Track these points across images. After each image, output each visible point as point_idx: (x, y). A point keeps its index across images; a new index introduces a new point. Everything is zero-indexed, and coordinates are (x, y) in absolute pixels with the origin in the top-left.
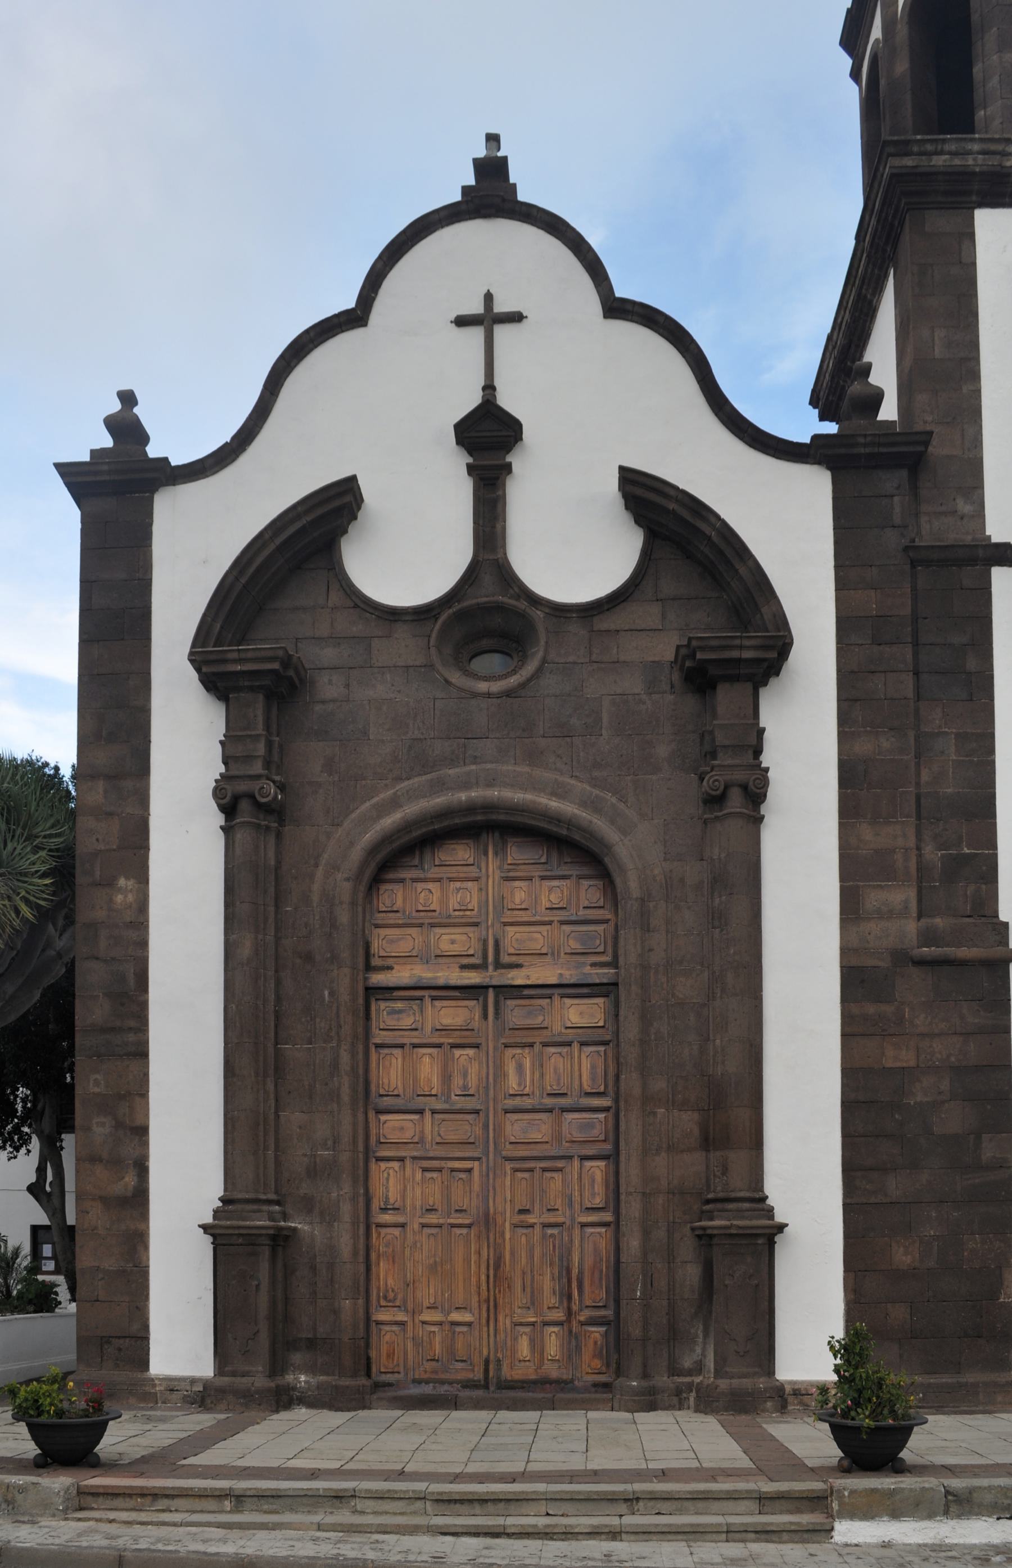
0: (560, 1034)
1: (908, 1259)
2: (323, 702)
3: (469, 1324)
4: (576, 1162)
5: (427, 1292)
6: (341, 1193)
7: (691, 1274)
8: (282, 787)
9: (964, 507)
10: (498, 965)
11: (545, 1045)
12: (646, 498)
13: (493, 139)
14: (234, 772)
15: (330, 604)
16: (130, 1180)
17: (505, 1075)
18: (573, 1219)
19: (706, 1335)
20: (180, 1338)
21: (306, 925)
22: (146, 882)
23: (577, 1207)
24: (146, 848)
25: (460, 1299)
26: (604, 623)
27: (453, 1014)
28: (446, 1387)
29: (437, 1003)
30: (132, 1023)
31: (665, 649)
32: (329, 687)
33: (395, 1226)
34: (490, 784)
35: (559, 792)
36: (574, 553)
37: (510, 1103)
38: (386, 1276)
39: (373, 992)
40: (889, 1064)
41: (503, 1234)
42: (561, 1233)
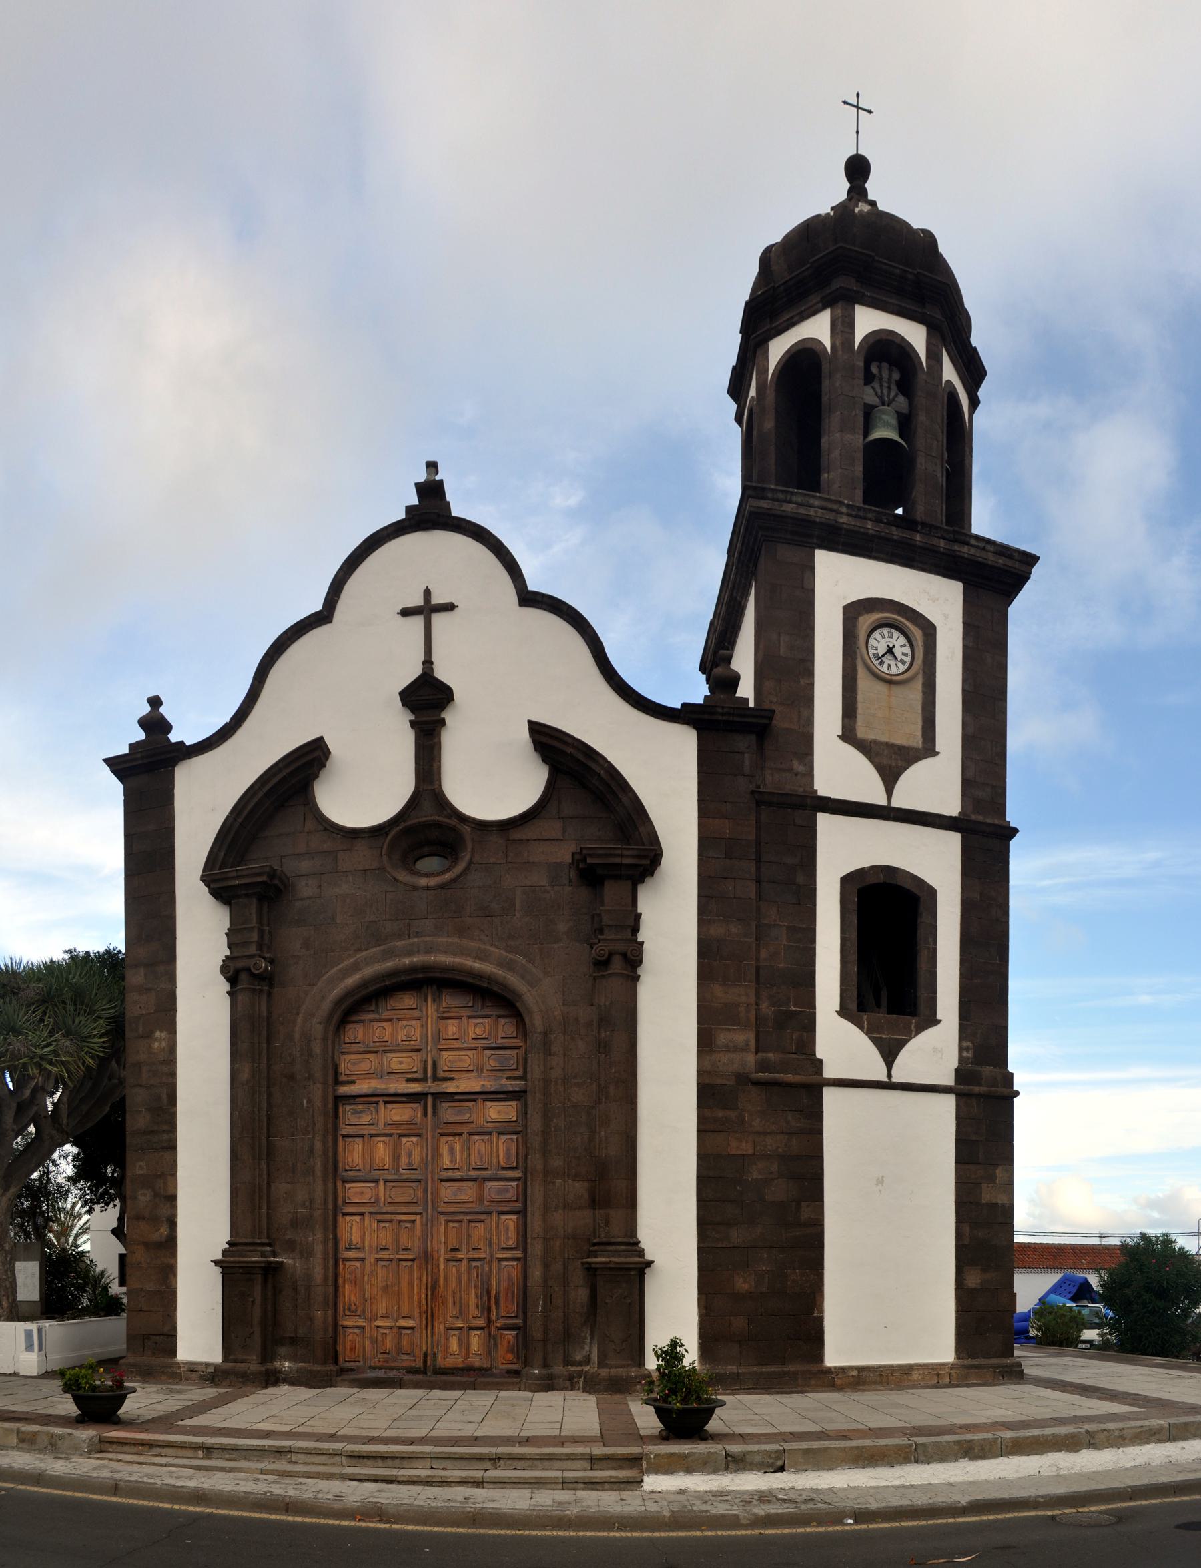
0: (483, 1126)
1: (746, 1286)
2: (302, 899)
3: (412, 1328)
4: (495, 1216)
5: (381, 1307)
6: (316, 1239)
7: (581, 1295)
8: (271, 962)
9: (798, 767)
10: (435, 1078)
11: (471, 1134)
12: (549, 742)
13: (432, 466)
14: (235, 955)
15: (306, 829)
16: (164, 1231)
17: (440, 1155)
18: (492, 1256)
19: (592, 1338)
20: (198, 1334)
21: (290, 1055)
22: (175, 1033)
23: (495, 1247)
24: (175, 1010)
25: (405, 1310)
26: (517, 835)
27: (400, 1114)
28: (394, 1372)
29: (389, 1106)
30: (166, 1127)
31: (564, 854)
32: (306, 889)
33: (357, 1260)
34: (428, 952)
35: (482, 956)
36: (493, 783)
37: (444, 1174)
38: (348, 1293)
39: (340, 1100)
40: (733, 1152)
41: (438, 1266)
42: (483, 1266)
